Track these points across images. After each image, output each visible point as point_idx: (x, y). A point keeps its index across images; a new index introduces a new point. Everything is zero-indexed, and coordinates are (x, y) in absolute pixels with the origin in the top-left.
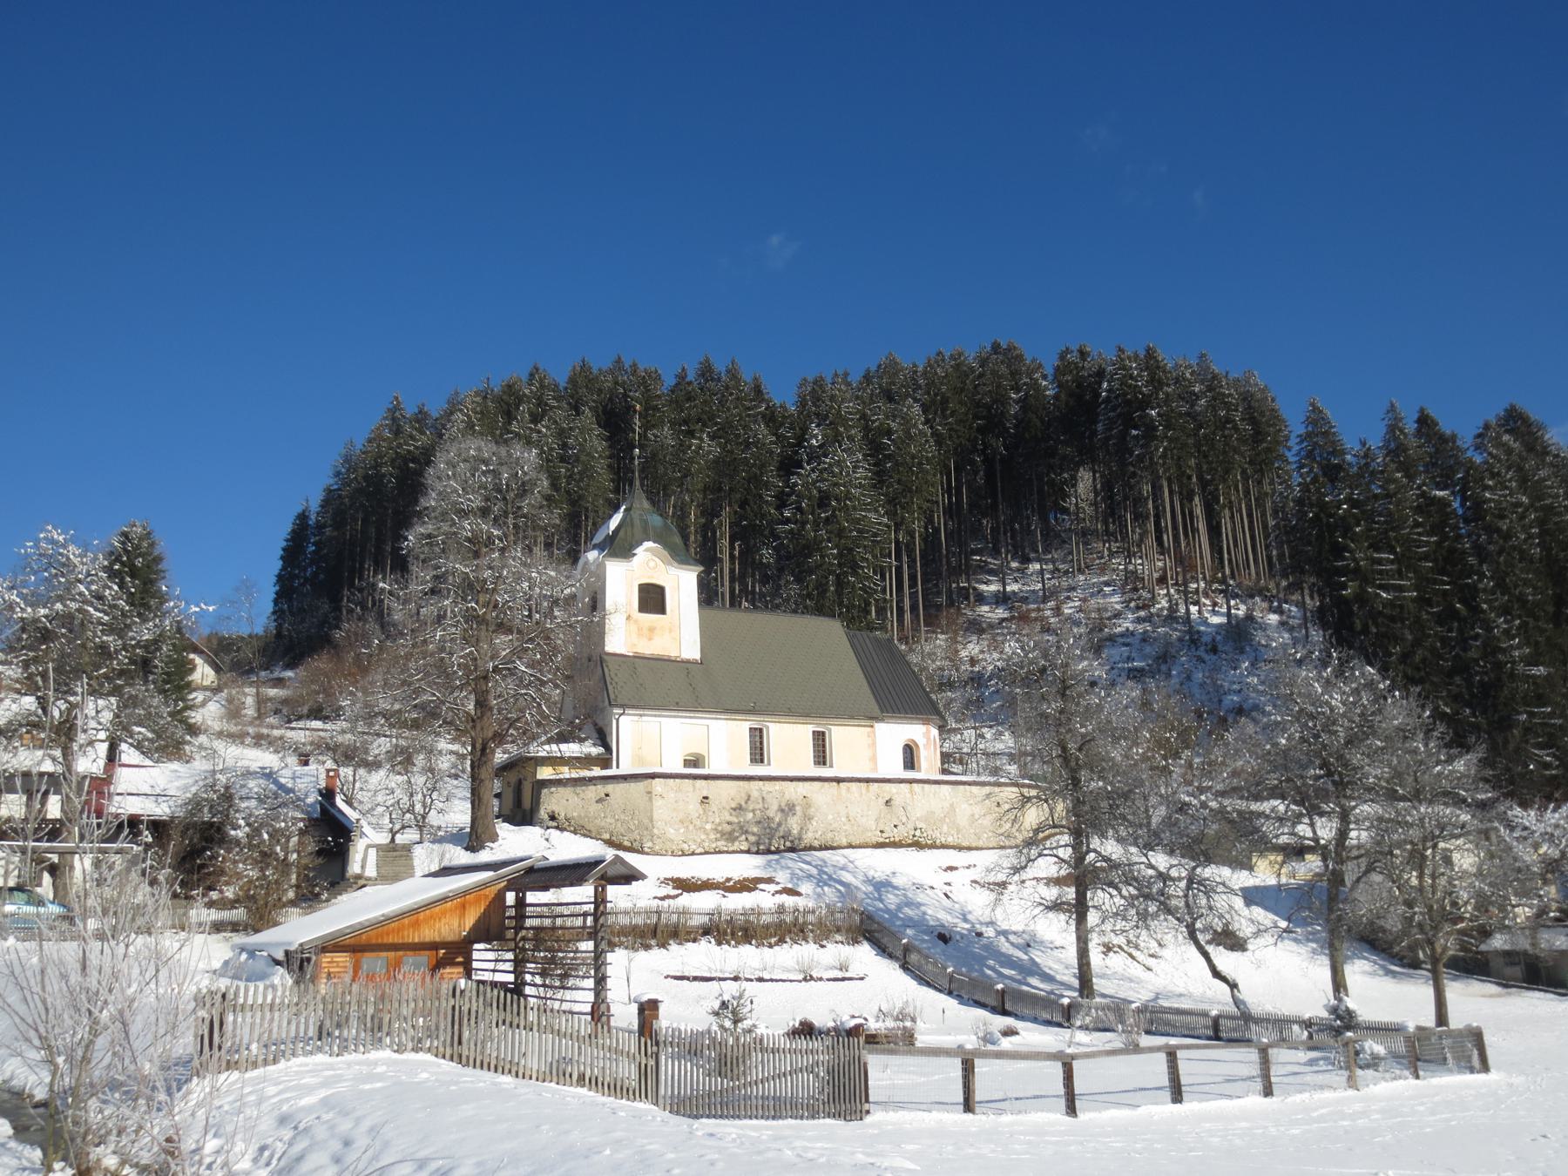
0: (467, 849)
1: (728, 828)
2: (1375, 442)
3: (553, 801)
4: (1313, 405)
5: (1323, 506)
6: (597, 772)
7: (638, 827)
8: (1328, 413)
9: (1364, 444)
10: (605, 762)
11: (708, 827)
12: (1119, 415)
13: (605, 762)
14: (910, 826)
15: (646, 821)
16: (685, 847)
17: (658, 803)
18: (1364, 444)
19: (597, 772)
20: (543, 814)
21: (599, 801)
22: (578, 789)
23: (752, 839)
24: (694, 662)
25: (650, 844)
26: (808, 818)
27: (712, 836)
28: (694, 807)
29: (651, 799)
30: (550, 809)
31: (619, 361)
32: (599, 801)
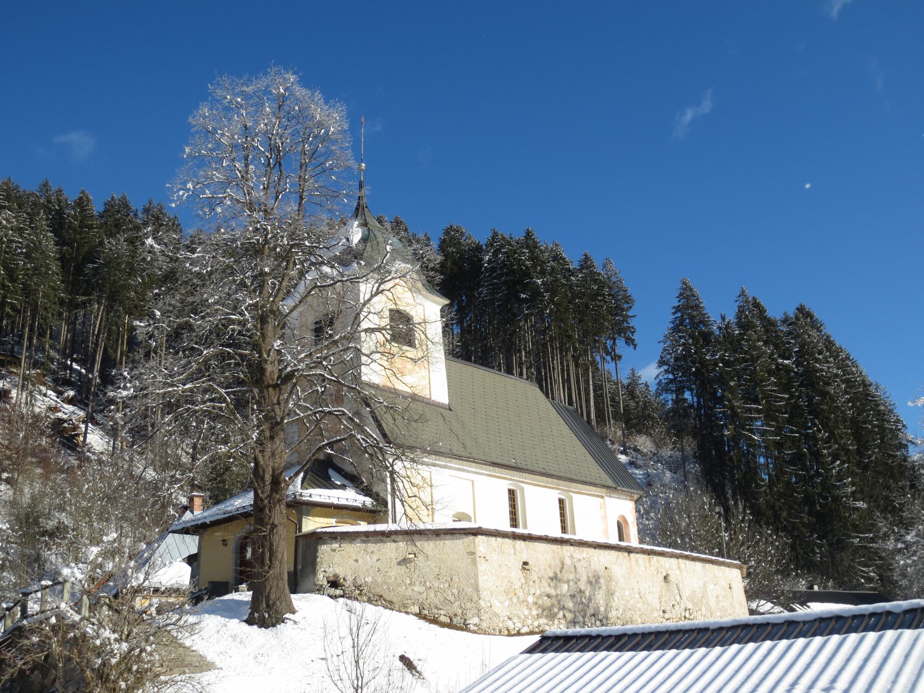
0: (250, 622)
1: (547, 602)
2: (731, 317)
3: (333, 560)
4: (684, 283)
5: (703, 362)
6: (363, 527)
7: (458, 597)
8: (697, 291)
9: (723, 318)
10: (375, 513)
11: (531, 599)
12: (505, 283)
13: (375, 513)
14: (683, 607)
15: (469, 590)
16: (510, 624)
17: (482, 566)
18: (723, 318)
19: (363, 527)
20: (321, 578)
21: (404, 562)
22: (371, 547)
23: (569, 616)
24: (438, 405)
25: (475, 620)
26: (610, 593)
27: (535, 612)
28: (516, 573)
29: (474, 562)
30: (331, 572)
31: (46, 185)
32: (404, 562)
